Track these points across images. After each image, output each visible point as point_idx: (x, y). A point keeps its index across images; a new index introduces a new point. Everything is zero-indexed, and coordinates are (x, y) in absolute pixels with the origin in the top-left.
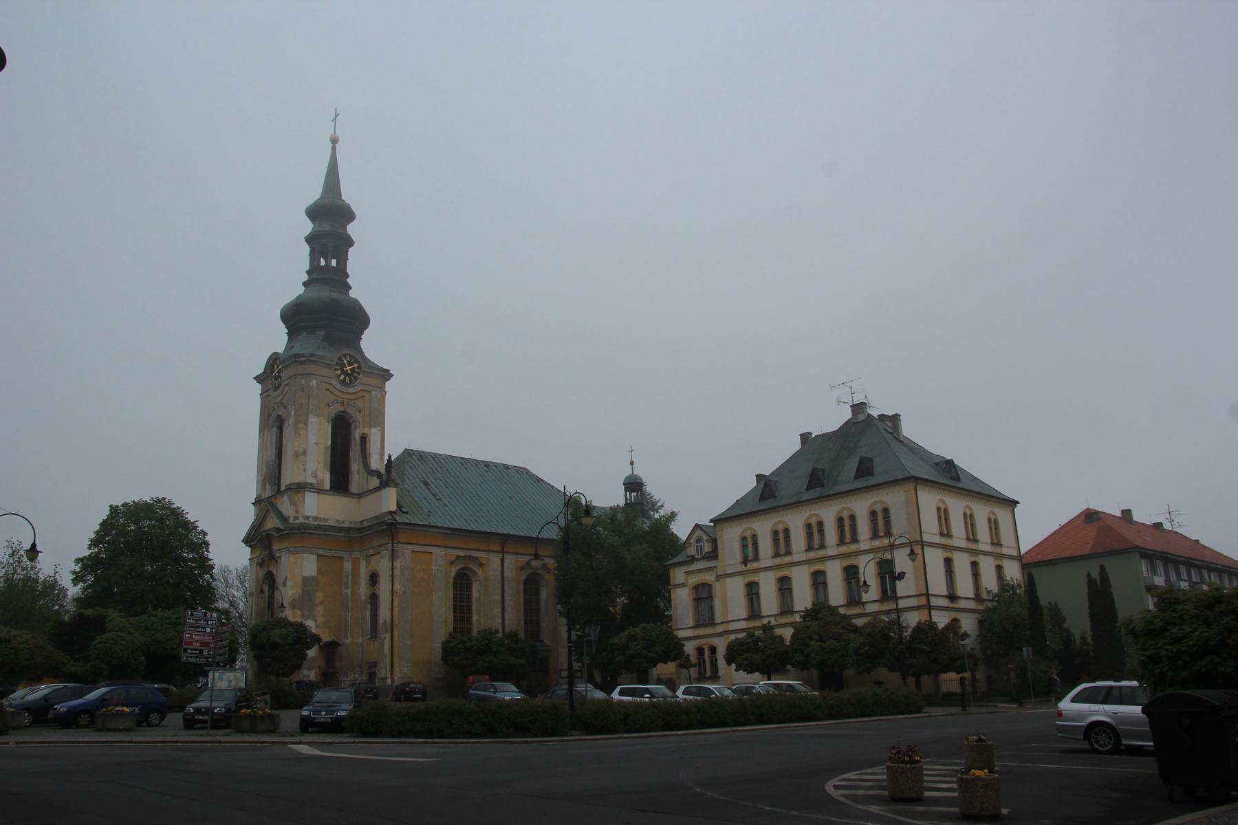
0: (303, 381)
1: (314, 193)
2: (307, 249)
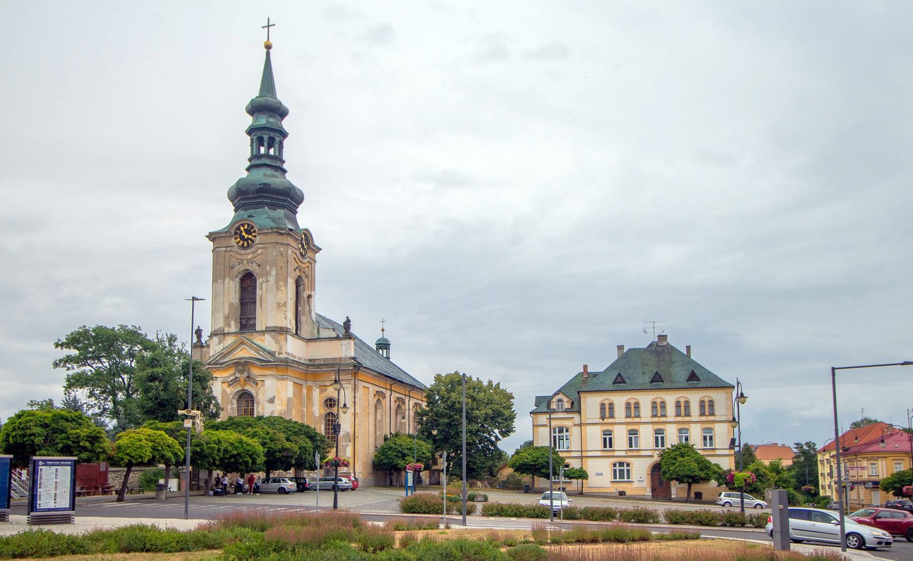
0: (282, 249)
1: (253, 91)
2: (248, 138)
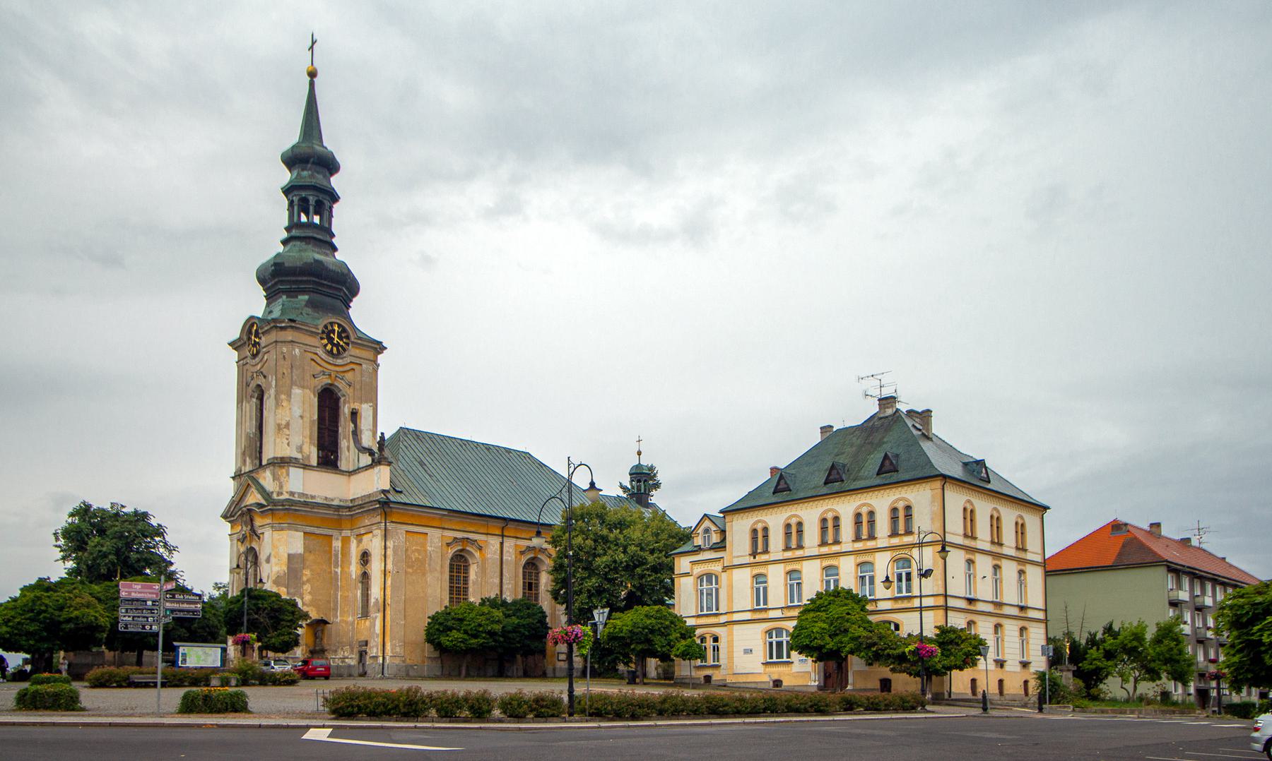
1: (291, 136)
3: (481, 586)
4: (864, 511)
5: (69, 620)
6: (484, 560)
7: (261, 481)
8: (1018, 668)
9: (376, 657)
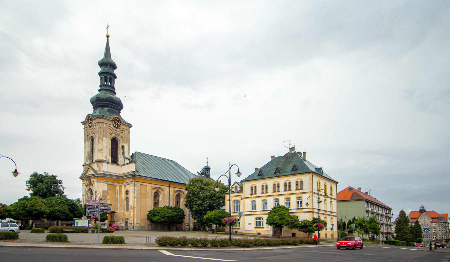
0: (101, 125)
1: (101, 57)
2: (99, 78)
3: (163, 202)
4: (287, 182)
5: (36, 210)
6: (164, 194)
7: (93, 167)
8: (330, 230)
9: (131, 224)
